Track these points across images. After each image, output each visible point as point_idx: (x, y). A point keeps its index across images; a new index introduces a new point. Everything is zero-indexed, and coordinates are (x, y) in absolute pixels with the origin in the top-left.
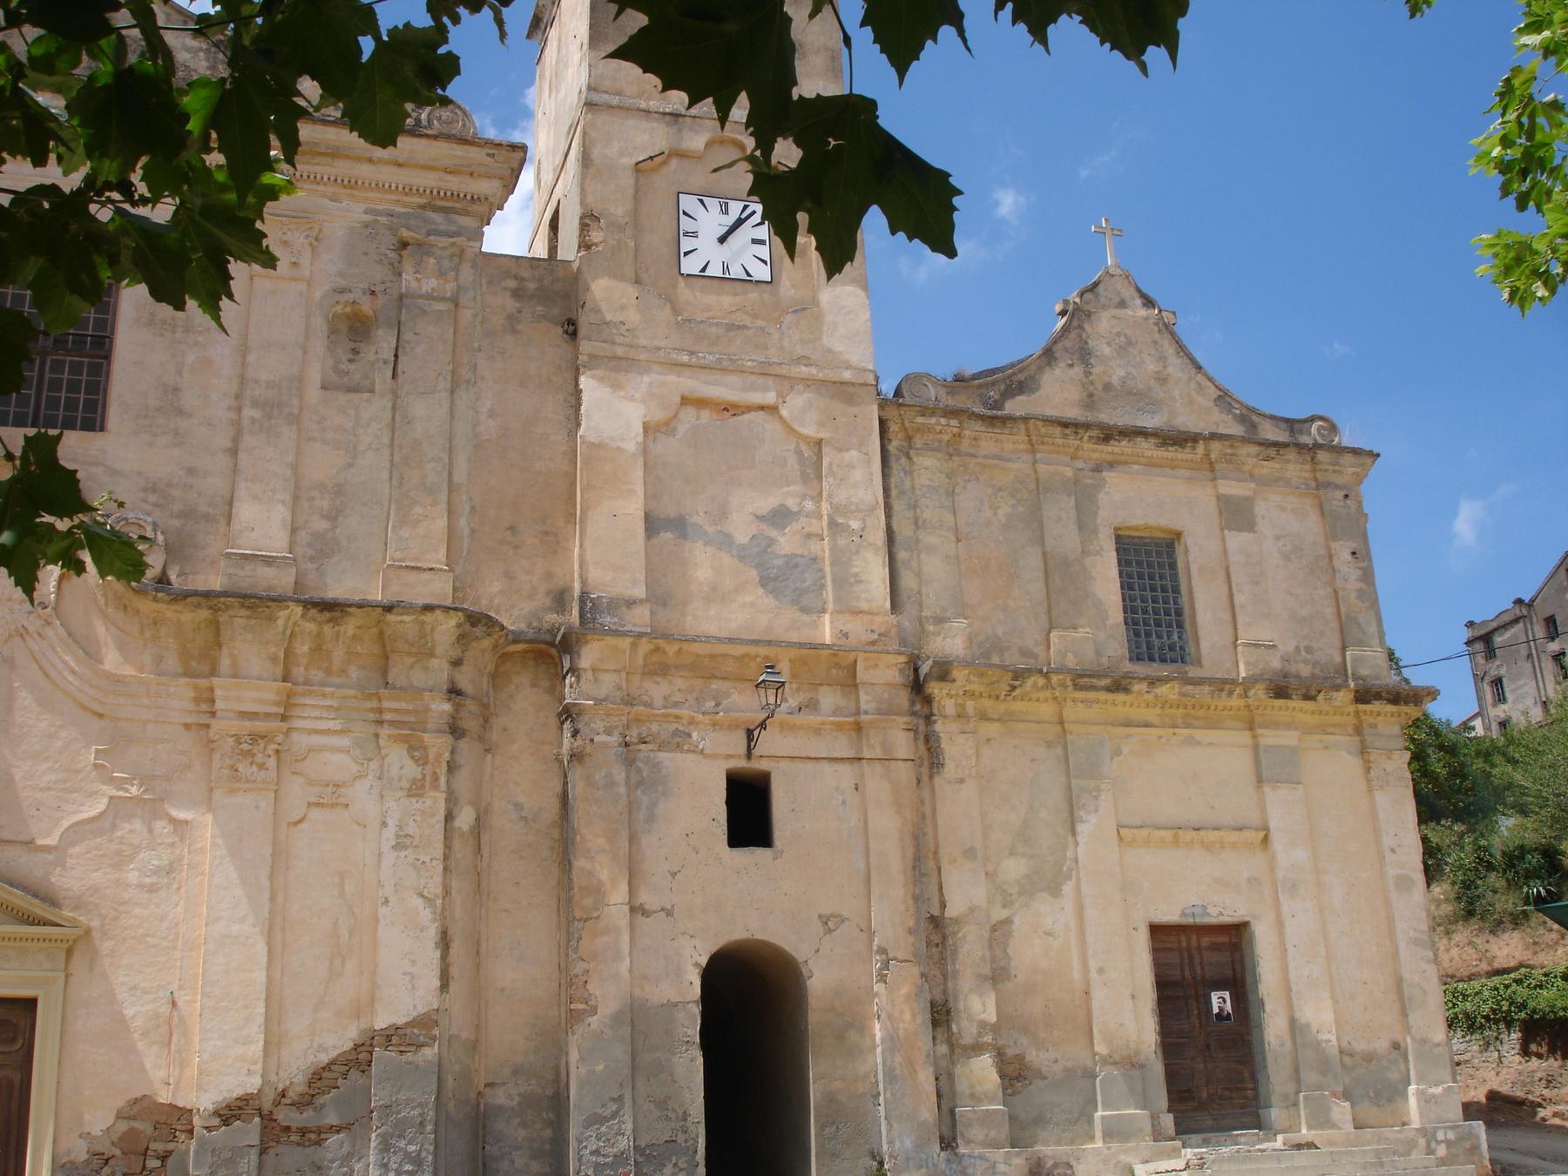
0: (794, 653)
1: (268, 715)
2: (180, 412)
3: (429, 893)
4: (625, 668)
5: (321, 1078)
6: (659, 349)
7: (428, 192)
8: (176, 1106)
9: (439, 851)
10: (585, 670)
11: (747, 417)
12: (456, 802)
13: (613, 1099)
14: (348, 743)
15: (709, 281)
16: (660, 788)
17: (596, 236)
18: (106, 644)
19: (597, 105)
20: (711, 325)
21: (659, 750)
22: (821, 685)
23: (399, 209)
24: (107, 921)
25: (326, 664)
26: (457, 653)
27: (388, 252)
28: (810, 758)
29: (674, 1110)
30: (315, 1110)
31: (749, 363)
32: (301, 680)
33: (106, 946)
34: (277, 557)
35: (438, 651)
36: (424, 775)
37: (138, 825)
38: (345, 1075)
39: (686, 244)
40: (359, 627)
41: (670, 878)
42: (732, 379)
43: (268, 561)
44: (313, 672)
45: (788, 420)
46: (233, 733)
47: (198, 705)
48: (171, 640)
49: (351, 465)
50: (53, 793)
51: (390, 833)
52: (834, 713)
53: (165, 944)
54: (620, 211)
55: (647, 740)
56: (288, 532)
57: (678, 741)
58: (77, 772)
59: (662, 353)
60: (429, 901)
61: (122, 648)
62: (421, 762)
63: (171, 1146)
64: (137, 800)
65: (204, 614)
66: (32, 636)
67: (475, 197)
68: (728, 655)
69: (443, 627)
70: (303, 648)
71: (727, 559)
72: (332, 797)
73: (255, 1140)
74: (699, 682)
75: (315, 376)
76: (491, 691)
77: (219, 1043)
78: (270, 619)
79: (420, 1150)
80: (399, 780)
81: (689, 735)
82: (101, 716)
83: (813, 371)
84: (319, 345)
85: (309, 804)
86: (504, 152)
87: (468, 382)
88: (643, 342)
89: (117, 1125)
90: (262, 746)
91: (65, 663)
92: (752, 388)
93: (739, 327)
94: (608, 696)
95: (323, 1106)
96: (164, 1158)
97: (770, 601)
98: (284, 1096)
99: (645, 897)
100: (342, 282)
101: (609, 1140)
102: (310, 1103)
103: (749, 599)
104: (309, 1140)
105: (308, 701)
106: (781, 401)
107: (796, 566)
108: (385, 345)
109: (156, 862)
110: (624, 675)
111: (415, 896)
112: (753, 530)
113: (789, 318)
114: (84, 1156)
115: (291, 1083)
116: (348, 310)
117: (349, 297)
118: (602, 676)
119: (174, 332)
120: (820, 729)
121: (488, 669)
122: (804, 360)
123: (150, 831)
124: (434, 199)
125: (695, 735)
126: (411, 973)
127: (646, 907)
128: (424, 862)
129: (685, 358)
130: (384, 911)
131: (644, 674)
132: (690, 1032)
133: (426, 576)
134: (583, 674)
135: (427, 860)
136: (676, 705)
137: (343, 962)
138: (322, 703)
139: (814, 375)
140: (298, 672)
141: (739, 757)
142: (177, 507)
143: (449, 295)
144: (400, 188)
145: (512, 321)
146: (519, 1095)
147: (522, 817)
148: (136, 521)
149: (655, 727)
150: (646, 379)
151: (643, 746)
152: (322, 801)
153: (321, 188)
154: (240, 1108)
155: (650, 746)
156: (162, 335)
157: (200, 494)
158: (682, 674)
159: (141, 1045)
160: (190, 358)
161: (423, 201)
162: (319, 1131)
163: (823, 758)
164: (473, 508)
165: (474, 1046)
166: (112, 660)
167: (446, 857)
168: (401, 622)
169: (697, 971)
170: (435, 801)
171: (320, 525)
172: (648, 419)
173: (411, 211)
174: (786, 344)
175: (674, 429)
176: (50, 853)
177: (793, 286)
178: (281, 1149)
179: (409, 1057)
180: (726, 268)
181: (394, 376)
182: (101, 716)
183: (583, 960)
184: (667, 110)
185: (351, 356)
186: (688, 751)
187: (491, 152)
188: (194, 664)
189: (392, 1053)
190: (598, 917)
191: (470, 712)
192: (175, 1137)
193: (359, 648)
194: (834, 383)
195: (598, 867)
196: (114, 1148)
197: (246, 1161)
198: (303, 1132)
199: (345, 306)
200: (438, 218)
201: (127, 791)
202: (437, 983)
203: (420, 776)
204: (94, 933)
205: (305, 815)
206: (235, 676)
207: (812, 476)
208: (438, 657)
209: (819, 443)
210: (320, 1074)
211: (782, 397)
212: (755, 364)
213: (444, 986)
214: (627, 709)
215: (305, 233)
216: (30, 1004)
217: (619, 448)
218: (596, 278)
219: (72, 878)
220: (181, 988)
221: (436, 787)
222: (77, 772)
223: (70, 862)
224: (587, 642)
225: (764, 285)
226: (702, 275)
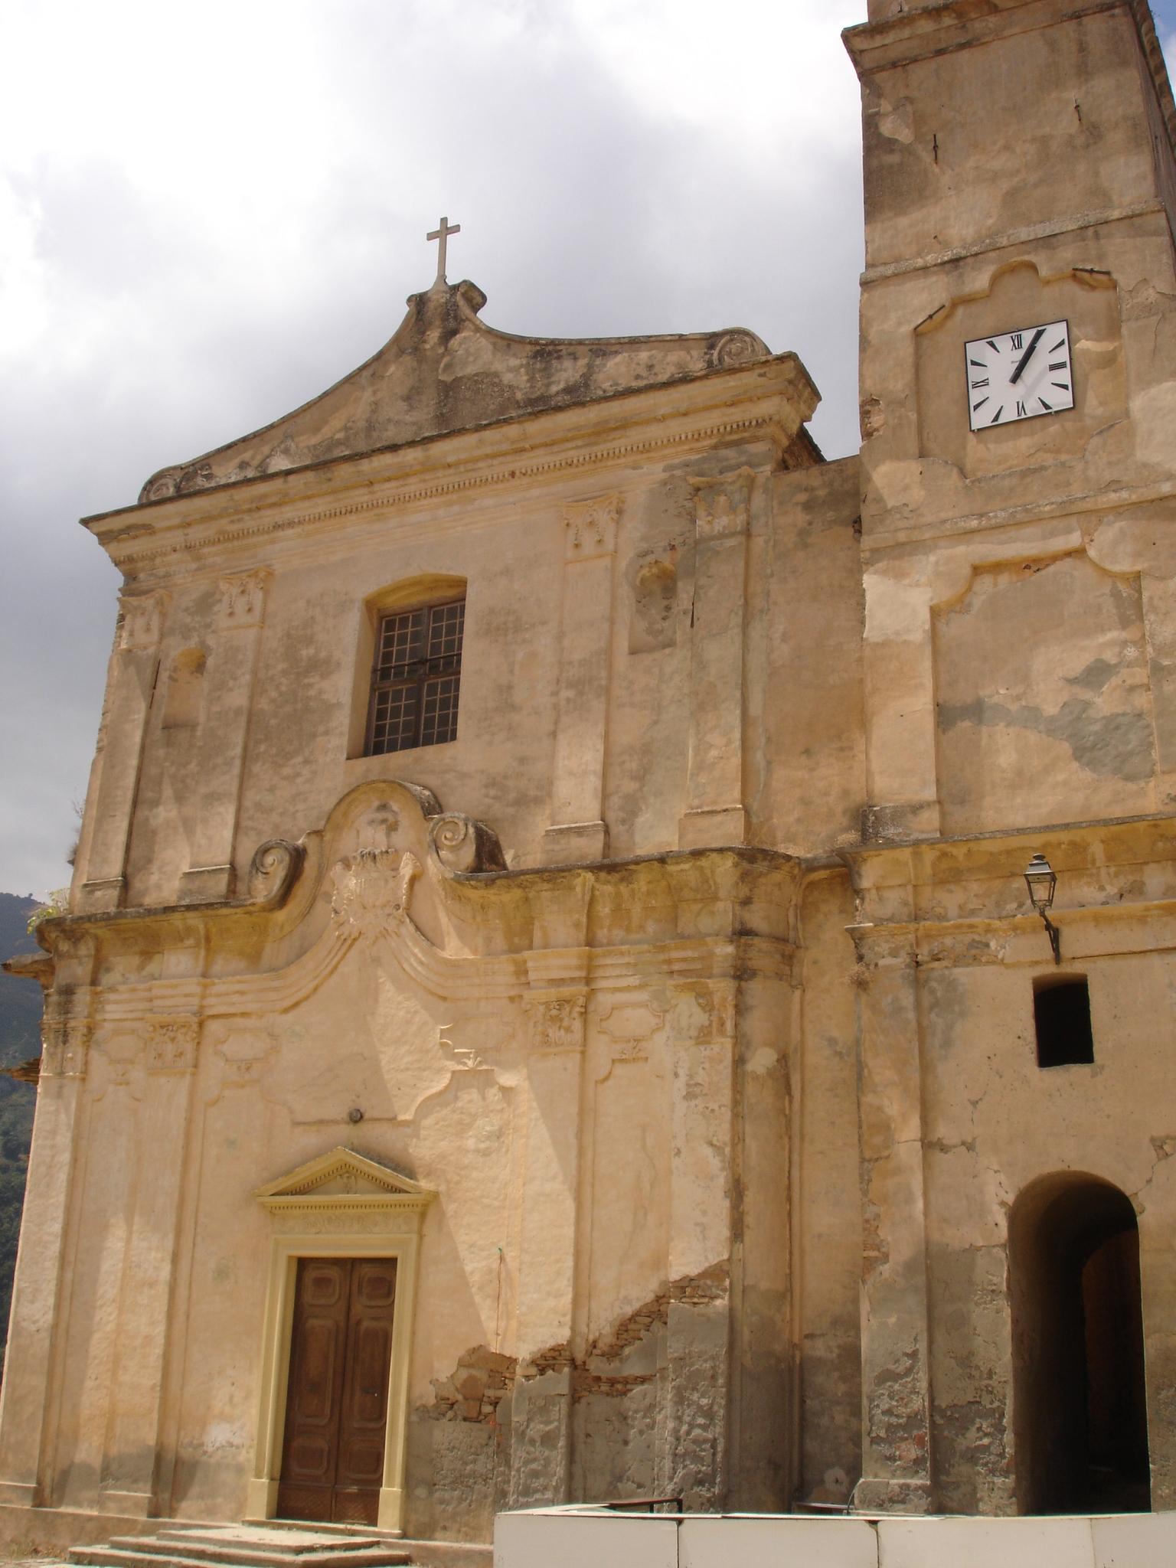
0: (1103, 832)
1: (573, 980)
2: (514, 708)
3: (718, 1140)
4: (910, 881)
5: (626, 1329)
6: (944, 522)
7: (715, 431)
8: (503, 1356)
9: (726, 1096)
10: (869, 890)
11: (1051, 569)
12: (748, 1045)
13: (907, 1355)
14: (647, 998)
15: (1003, 429)
16: (957, 1008)
17: (876, 420)
18: (448, 934)
19: (873, 281)
20: (1003, 477)
21: (955, 966)
22: (1147, 863)
23: (695, 457)
24: (451, 1186)
25: (626, 923)
26: (744, 891)
27: (686, 503)
28: (1135, 953)
29: (977, 1367)
30: (621, 1360)
31: (1047, 508)
32: (605, 941)
33: (450, 1208)
34: (588, 827)
35: (722, 894)
36: (711, 1021)
37: (474, 1094)
38: (648, 1328)
39: (975, 396)
40: (649, 882)
41: (970, 1108)
42: (1029, 531)
43: (579, 831)
44: (615, 932)
45: (1097, 561)
46: (544, 1001)
47: (518, 978)
48: (497, 921)
49: (656, 722)
50: (410, 1073)
51: (681, 1083)
52: (1164, 894)
53: (496, 1203)
54: (900, 386)
55: (941, 956)
56: (599, 800)
57: (976, 953)
58: (428, 1051)
59: (948, 526)
60: (718, 1149)
61: (461, 936)
62: (707, 1009)
63: (500, 1393)
64: (473, 1072)
65: (517, 893)
66: (391, 936)
67: (760, 421)
68: (1027, 848)
69: (722, 869)
70: (604, 910)
71: (1032, 737)
72: (633, 1052)
73: (564, 1388)
74: (998, 884)
75: (623, 644)
76: (799, 925)
77: (535, 1296)
78: (570, 888)
79: (712, 1404)
80: (688, 1030)
81: (987, 945)
82: (444, 999)
83: (1124, 494)
84: (626, 611)
85: (613, 1061)
86: (774, 367)
87: (762, 611)
88: (929, 519)
89: (459, 1372)
90: (568, 1009)
91: (415, 955)
92: (1053, 534)
93: (1036, 471)
94: (893, 915)
95: (628, 1357)
96: (495, 1404)
97: (1087, 775)
98: (595, 1347)
99: (943, 1131)
100: (645, 545)
101: (902, 1399)
102: (617, 1355)
103: (1061, 777)
104: (617, 1390)
105: (608, 961)
106: (1087, 540)
107: (1117, 728)
108: (685, 596)
109: (488, 1128)
110: (910, 888)
111: (705, 1145)
112: (1065, 697)
113: (1095, 441)
114: (432, 1401)
115: (600, 1334)
116: (655, 570)
117: (650, 558)
118: (887, 894)
119: (506, 635)
120: (1145, 917)
121: (793, 903)
122: (1114, 485)
123: (484, 1099)
124: (723, 435)
125: (993, 944)
126: (702, 1224)
127: (944, 1142)
128: (713, 1111)
129: (974, 523)
130: (676, 1162)
131: (934, 884)
132: (995, 1280)
133: (719, 818)
134: (867, 895)
135: (716, 1107)
136: (973, 913)
137: (645, 1215)
138: (620, 961)
139: (1126, 499)
140: (602, 934)
141: (1047, 962)
142: (512, 796)
143: (739, 528)
144: (690, 437)
145: (803, 534)
146: (839, 1347)
147: (836, 1052)
148: (451, 819)
149: (948, 941)
150: (932, 558)
151: (936, 964)
152: (624, 1057)
153: (622, 460)
154: (554, 1358)
155: (944, 963)
156: (497, 641)
157: (529, 780)
158: (978, 877)
159: (477, 1299)
160: (520, 656)
161: (713, 441)
162: (626, 1381)
163: (1151, 951)
164: (769, 740)
165: (785, 1295)
166: (454, 949)
167: (736, 1103)
168: (682, 870)
169: (1003, 1210)
170: (723, 1047)
171: (630, 786)
172: (935, 602)
173: (705, 454)
174: (1091, 473)
175: (970, 605)
176: (408, 1127)
177: (1101, 404)
178: (592, 1398)
179: (700, 1309)
180: (1021, 408)
181: (692, 626)
182: (444, 999)
183: (874, 1204)
184: (946, 258)
185: (664, 614)
186: (988, 963)
187: (762, 371)
188: (516, 940)
189: (686, 1305)
190: (888, 1157)
191: (760, 951)
192: (505, 1384)
193: (653, 902)
194: (1153, 501)
195: (886, 1102)
196: (456, 1394)
197: (557, 1409)
198: (612, 1382)
199: (650, 568)
200: (730, 453)
201: (465, 1064)
202: (726, 1233)
203: (707, 1023)
204: (441, 1196)
205: (610, 1073)
206: (545, 947)
207: (1134, 617)
208: (721, 900)
209: (1138, 576)
210: (626, 1325)
211: (1087, 533)
212: (1054, 506)
213: (738, 1230)
214: (912, 926)
215: (607, 510)
216: (391, 1263)
217: (905, 642)
218: (877, 466)
219: (422, 1149)
220: (509, 1244)
221: (722, 1032)
222: (428, 1051)
223: (423, 1133)
224: (865, 860)
225: (1067, 413)
226: (996, 426)
